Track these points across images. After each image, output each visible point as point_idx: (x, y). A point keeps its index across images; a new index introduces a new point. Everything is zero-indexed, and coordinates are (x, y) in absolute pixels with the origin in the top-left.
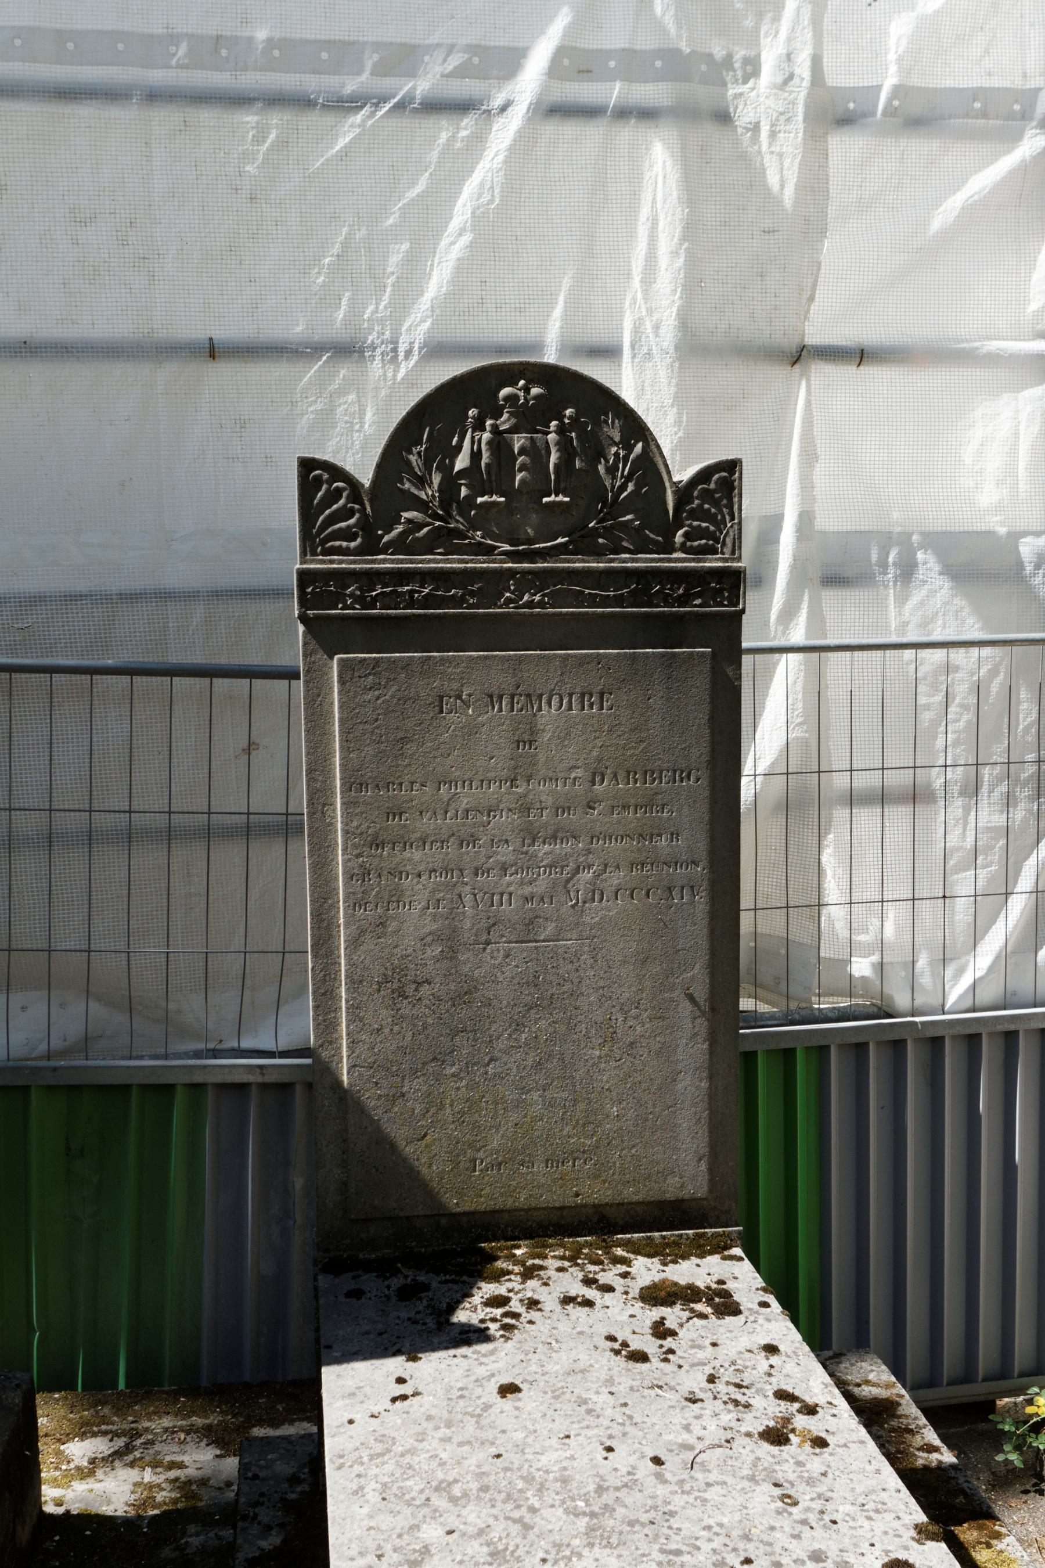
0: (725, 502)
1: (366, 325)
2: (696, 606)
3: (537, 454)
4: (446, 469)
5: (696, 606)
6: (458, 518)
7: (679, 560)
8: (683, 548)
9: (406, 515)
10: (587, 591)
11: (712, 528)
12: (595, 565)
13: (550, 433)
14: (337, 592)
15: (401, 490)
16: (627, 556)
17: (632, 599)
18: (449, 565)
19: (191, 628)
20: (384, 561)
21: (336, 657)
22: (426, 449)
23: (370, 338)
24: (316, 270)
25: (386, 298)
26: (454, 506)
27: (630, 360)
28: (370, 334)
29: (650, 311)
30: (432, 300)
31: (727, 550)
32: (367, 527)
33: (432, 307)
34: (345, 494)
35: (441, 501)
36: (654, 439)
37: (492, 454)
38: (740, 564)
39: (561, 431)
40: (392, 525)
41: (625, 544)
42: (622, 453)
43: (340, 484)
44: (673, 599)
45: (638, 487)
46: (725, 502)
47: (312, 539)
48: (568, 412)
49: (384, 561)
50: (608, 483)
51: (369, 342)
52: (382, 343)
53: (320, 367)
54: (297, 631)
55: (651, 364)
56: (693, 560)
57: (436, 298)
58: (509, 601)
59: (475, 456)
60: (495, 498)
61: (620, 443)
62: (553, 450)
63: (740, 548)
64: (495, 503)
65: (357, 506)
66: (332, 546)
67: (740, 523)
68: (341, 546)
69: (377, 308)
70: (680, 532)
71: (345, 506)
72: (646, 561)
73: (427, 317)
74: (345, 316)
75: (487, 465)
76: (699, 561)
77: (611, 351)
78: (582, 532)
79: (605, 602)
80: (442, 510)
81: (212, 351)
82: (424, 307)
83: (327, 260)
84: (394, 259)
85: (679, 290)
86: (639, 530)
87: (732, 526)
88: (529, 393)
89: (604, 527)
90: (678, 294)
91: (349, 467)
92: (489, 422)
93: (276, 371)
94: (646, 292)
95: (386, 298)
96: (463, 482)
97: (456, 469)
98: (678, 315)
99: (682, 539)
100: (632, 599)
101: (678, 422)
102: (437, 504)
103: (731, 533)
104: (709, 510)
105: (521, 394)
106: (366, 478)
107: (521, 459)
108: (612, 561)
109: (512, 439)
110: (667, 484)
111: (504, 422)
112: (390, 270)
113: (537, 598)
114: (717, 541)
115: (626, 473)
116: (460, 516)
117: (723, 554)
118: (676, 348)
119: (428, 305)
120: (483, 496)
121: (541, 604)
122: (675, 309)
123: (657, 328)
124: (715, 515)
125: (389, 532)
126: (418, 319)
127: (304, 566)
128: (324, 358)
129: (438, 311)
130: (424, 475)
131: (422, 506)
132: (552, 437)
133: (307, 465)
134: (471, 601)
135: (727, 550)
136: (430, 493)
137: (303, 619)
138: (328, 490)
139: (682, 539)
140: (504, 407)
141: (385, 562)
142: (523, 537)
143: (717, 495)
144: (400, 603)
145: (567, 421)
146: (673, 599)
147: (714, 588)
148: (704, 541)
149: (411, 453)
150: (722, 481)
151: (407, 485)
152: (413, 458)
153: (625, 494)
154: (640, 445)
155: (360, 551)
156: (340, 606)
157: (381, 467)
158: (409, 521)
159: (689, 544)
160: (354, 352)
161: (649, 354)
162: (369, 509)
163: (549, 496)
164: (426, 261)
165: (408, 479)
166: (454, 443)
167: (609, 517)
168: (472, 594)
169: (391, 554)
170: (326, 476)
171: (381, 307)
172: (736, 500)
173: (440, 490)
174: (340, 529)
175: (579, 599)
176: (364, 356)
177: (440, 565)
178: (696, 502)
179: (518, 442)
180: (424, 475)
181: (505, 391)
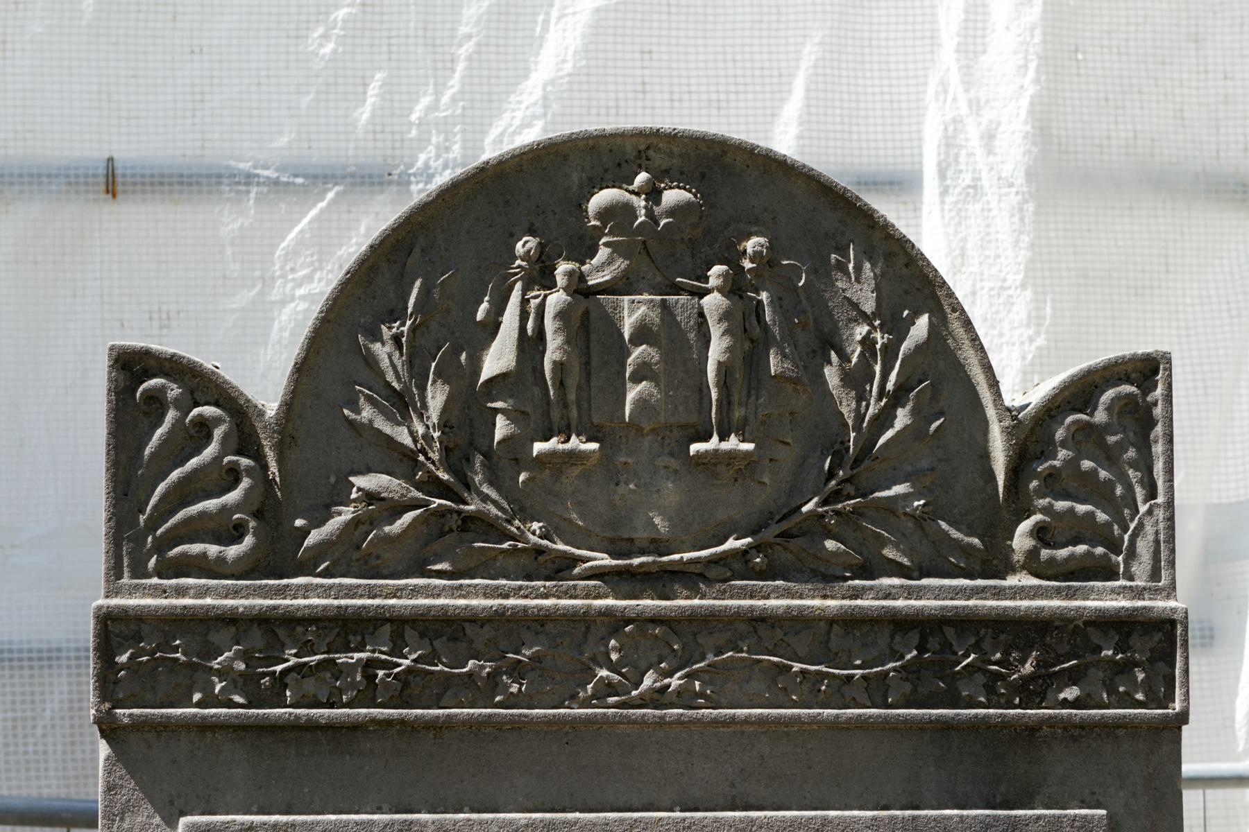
0: (1131, 453)
1: (414, 133)
2: (1066, 704)
3: (677, 342)
4: (462, 379)
5: (1066, 704)
6: (486, 489)
7: (1022, 594)
8: (1033, 565)
9: (360, 481)
10: (797, 667)
11: (1102, 517)
12: (817, 602)
13: (708, 292)
14: (189, 665)
15: (351, 424)
16: (896, 581)
17: (908, 687)
18: (462, 602)
19: (40, 723)
20: (306, 591)
21: (184, 821)
22: (413, 329)
23: (422, 157)
24: (320, 31)
25: (455, 82)
26: (479, 459)
27: (937, 199)
28: (422, 149)
29: (976, 106)
30: (545, 86)
31: (1141, 568)
32: (267, 509)
33: (545, 98)
34: (218, 433)
35: (446, 450)
36: (958, 308)
37: (568, 341)
38: (1172, 604)
39: (735, 288)
40: (328, 507)
41: (889, 553)
42: (880, 339)
43: (209, 410)
44: (1010, 686)
45: (921, 417)
46: (1131, 453)
47: (135, 536)
48: (752, 244)
49: (306, 591)
50: (847, 409)
51: (420, 164)
52: (445, 167)
53: (322, 211)
54: (95, 751)
55: (978, 207)
56: (1058, 593)
57: (552, 82)
58: (609, 688)
59: (531, 345)
60: (575, 443)
61: (875, 315)
62: (716, 331)
63: (1172, 564)
64: (574, 456)
65: (245, 462)
66: (184, 555)
67: (1170, 505)
68: (204, 555)
69: (437, 101)
70: (1025, 526)
71: (217, 459)
72: (936, 596)
73: (534, 117)
74: (373, 116)
75: (559, 366)
76: (1071, 594)
77: (900, 183)
78: (785, 525)
79: (842, 693)
80: (448, 470)
81: (112, 182)
82: (528, 99)
83: (342, 13)
84: (473, 10)
85: (1033, 66)
86: (920, 520)
87: (1150, 512)
88: (658, 201)
89: (837, 513)
90: (1031, 74)
91: (231, 374)
92: (563, 268)
93: (232, 219)
94: (967, 71)
95: (455, 82)
96: (499, 405)
97: (485, 375)
98: (1031, 112)
99: (1029, 543)
100: (908, 687)
101: (1035, 319)
102: (435, 456)
103: (1149, 529)
104: (1094, 472)
105: (640, 203)
106: (266, 390)
107: (637, 353)
108: (856, 594)
109: (617, 307)
110: (991, 412)
111: (599, 269)
112: (463, 30)
113: (675, 682)
114: (1115, 547)
115: (890, 386)
116: (491, 484)
117: (1131, 579)
118: (1030, 175)
119: (537, 94)
120: (546, 439)
121: (685, 698)
122: (1025, 102)
123: (989, 137)
124: (1110, 485)
125: (322, 523)
126: (517, 122)
127: (115, 602)
128: (330, 195)
129: (556, 107)
130: (407, 388)
131: (403, 461)
132: (713, 302)
133: (131, 366)
134: (514, 688)
135: (1141, 568)
136: (421, 430)
137: (109, 729)
138: (178, 422)
139: (1029, 543)
140: (599, 232)
141: (309, 594)
142: (641, 535)
143: (1112, 439)
144: (341, 691)
145: (747, 265)
146: (1010, 686)
147: (1110, 661)
148: (1082, 548)
149: (377, 337)
150: (1121, 407)
151: (367, 413)
152: (382, 351)
153: (889, 434)
154: (923, 321)
155: (251, 568)
156: (197, 697)
157: (305, 370)
158: (370, 497)
159: (1045, 553)
160: (390, 183)
161: (975, 187)
162: (273, 468)
163: (707, 438)
164: (535, 14)
165: (370, 399)
166: (480, 315)
167: (849, 489)
168: (517, 670)
169: (325, 574)
170: (174, 391)
171: (445, 99)
172: (1158, 449)
173: (444, 425)
174: (203, 514)
175: (779, 685)
176: (408, 191)
177: (441, 601)
178: (1062, 454)
179: (632, 312)
180: (407, 388)
181: (603, 198)
